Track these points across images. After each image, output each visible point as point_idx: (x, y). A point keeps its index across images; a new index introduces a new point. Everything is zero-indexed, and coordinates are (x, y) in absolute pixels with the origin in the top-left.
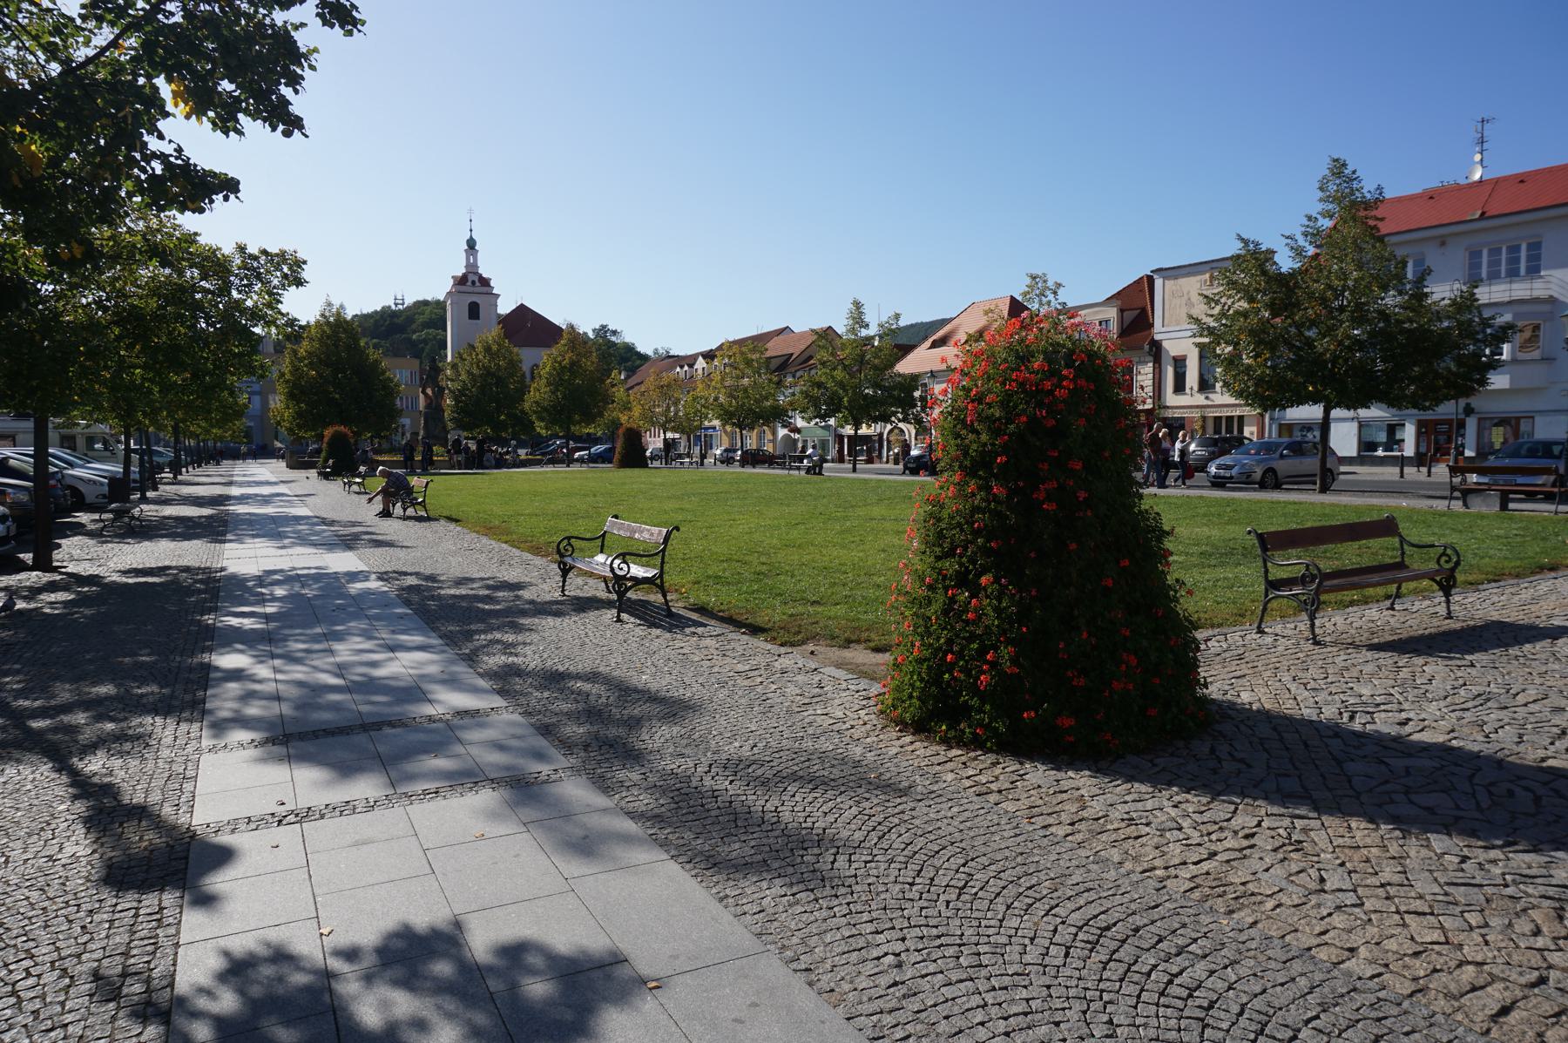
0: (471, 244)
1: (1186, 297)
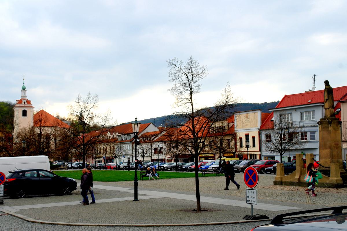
0: (24, 89)
1: (242, 121)
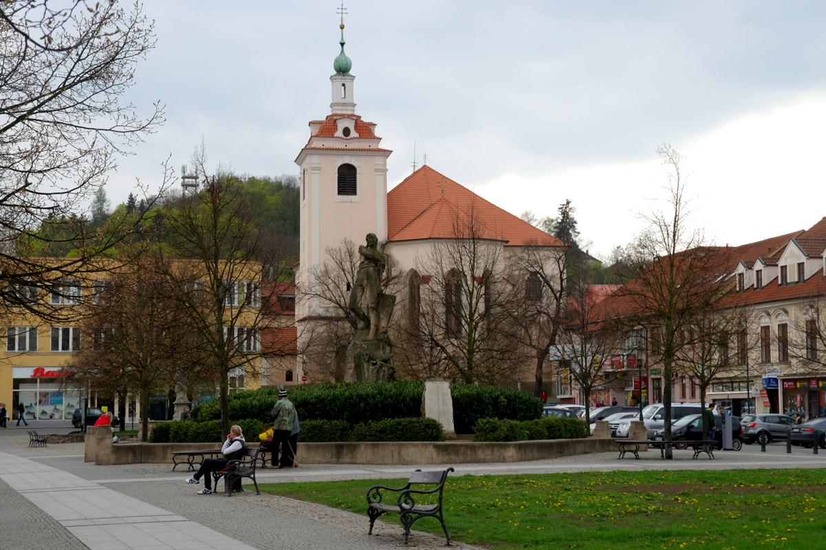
0: (342, 70)
